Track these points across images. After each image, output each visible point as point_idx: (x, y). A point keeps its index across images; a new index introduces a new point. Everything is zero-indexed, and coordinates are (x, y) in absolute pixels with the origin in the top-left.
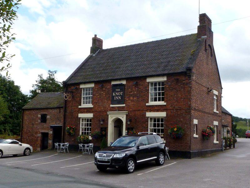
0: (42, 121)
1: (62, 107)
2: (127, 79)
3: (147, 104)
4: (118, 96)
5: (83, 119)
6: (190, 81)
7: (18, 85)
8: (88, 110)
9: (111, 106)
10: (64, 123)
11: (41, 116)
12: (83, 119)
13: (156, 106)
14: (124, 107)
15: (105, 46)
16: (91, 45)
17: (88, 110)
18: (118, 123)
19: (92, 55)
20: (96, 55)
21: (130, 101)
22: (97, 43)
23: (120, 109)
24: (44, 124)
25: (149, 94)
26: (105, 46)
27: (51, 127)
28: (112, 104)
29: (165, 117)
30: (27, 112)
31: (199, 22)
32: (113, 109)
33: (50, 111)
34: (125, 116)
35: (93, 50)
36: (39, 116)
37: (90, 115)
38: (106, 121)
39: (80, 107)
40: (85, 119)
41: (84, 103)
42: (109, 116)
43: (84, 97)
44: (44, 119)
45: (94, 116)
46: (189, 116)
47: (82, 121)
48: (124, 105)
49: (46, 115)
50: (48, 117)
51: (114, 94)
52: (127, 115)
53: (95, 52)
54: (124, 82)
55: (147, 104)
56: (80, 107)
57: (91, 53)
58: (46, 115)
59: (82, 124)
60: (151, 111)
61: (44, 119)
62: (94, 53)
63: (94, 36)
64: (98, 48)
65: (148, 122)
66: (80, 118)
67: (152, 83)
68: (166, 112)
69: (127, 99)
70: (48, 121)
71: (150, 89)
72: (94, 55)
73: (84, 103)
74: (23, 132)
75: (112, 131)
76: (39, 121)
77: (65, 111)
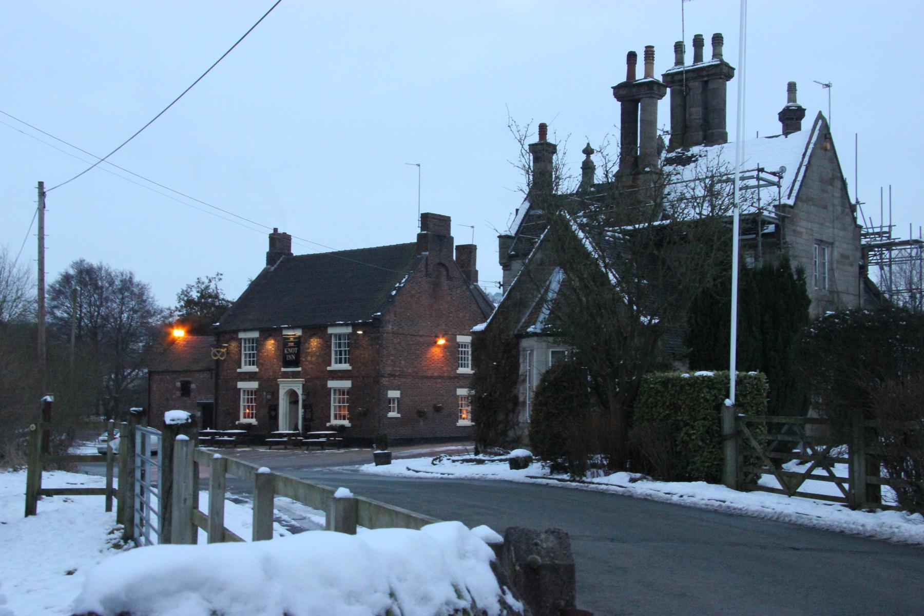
0: (183, 395)
1: (213, 369)
3: (329, 368)
4: (291, 354)
5: (335, 390)
6: (378, 335)
7: (724, 45)
8: (250, 376)
9: (283, 369)
10: (216, 399)
11: (182, 385)
12: (335, 390)
13: (339, 371)
14: (299, 371)
15: (298, 249)
16: (268, 250)
17: (250, 376)
18: (293, 394)
19: (269, 268)
20: (275, 269)
21: (307, 363)
22: (278, 245)
23: (295, 375)
24: (186, 399)
25: (331, 353)
26: (298, 249)
27: (199, 404)
28: (284, 367)
29: (350, 388)
30: (157, 377)
31: (581, 168)
32: (286, 375)
33: (197, 375)
34: (301, 385)
35: (271, 258)
36: (178, 384)
37: (254, 385)
38: (275, 394)
39: (239, 370)
40: (339, 391)
41: (245, 365)
42: (281, 385)
43: (246, 354)
45: (259, 385)
46: (378, 386)
47: (335, 394)
48: (300, 369)
49: (189, 383)
50: (193, 386)
51: (286, 351)
52: (304, 385)
53: (275, 263)
55: (329, 368)
56: (239, 370)
57: (268, 263)
58: (189, 383)
59: (334, 398)
60: (333, 379)
62: (272, 266)
63: (272, 232)
64: (279, 254)
65: (330, 395)
66: (331, 388)
67: (336, 335)
68: (352, 380)
69: (304, 359)
70: (192, 394)
71: (333, 344)
72: (273, 268)
73: (245, 365)
74: (151, 414)
75: (286, 410)
76: (178, 393)
77: (217, 376)
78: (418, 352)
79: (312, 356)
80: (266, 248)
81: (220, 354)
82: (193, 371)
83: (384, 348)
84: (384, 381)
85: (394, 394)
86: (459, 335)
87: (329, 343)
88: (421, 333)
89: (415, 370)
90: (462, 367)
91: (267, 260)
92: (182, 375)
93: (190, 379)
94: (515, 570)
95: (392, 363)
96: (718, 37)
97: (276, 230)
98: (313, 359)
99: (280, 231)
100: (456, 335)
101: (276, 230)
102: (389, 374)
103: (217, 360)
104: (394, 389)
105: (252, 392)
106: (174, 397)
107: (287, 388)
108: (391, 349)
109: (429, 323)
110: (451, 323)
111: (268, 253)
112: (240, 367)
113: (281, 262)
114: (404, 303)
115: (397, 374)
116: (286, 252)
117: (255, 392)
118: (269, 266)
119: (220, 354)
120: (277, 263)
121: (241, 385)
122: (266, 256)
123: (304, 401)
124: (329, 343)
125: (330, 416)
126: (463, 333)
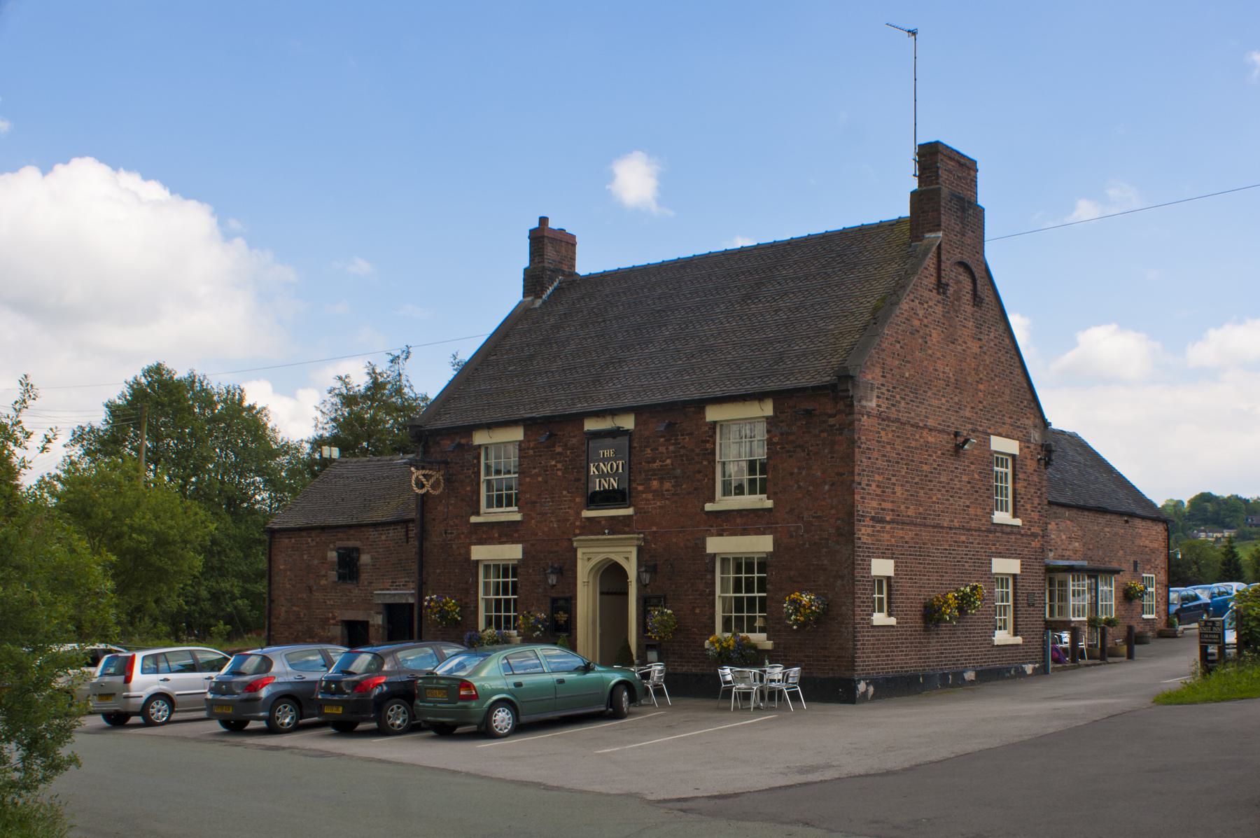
0: (342, 577)
1: (412, 521)
2: (637, 411)
8: (503, 533)
12: (487, 567)
15: (586, 265)
16: (527, 264)
18: (612, 575)
21: (650, 496)
22: (550, 252)
23: (617, 525)
26: (586, 265)
30: (287, 541)
32: (593, 527)
33: (373, 534)
34: (634, 551)
35: (533, 281)
36: (333, 555)
37: (512, 552)
38: (567, 571)
39: (474, 519)
44: (348, 567)
48: (629, 511)
50: (365, 559)
52: (640, 551)
53: (543, 290)
54: (628, 423)
61: (348, 567)
62: (539, 296)
63: (536, 225)
65: (714, 572)
69: (640, 488)
70: (364, 576)
72: (538, 303)
73: (490, 505)
76: (333, 575)
77: (423, 536)
78: (925, 468)
79: (661, 480)
80: (522, 258)
81: (432, 481)
82: (367, 525)
83: (863, 453)
84: (864, 532)
85: (882, 567)
86: (475, 544)
87: (709, 446)
88: (930, 423)
89: (921, 510)
90: (1002, 510)
91: (524, 286)
92: (340, 535)
93: (358, 544)
94: (121, 458)
95: (879, 491)
96: (969, 169)
97: (543, 221)
98: (667, 485)
99: (553, 224)
100: (989, 435)
101: (543, 221)
102: (873, 519)
103: (423, 495)
104: (883, 556)
105: (506, 569)
106: (323, 582)
107: (597, 559)
108: (875, 455)
109: (944, 400)
110: (981, 406)
111: (526, 270)
112: (478, 514)
113: (555, 289)
114: (898, 346)
115: (888, 518)
116: (565, 268)
117: (515, 568)
118: (529, 299)
119: (432, 481)
120: (549, 292)
121: (479, 552)
122: (522, 276)
123: (641, 586)
124: (709, 446)
125: (714, 622)
126: (1000, 430)
